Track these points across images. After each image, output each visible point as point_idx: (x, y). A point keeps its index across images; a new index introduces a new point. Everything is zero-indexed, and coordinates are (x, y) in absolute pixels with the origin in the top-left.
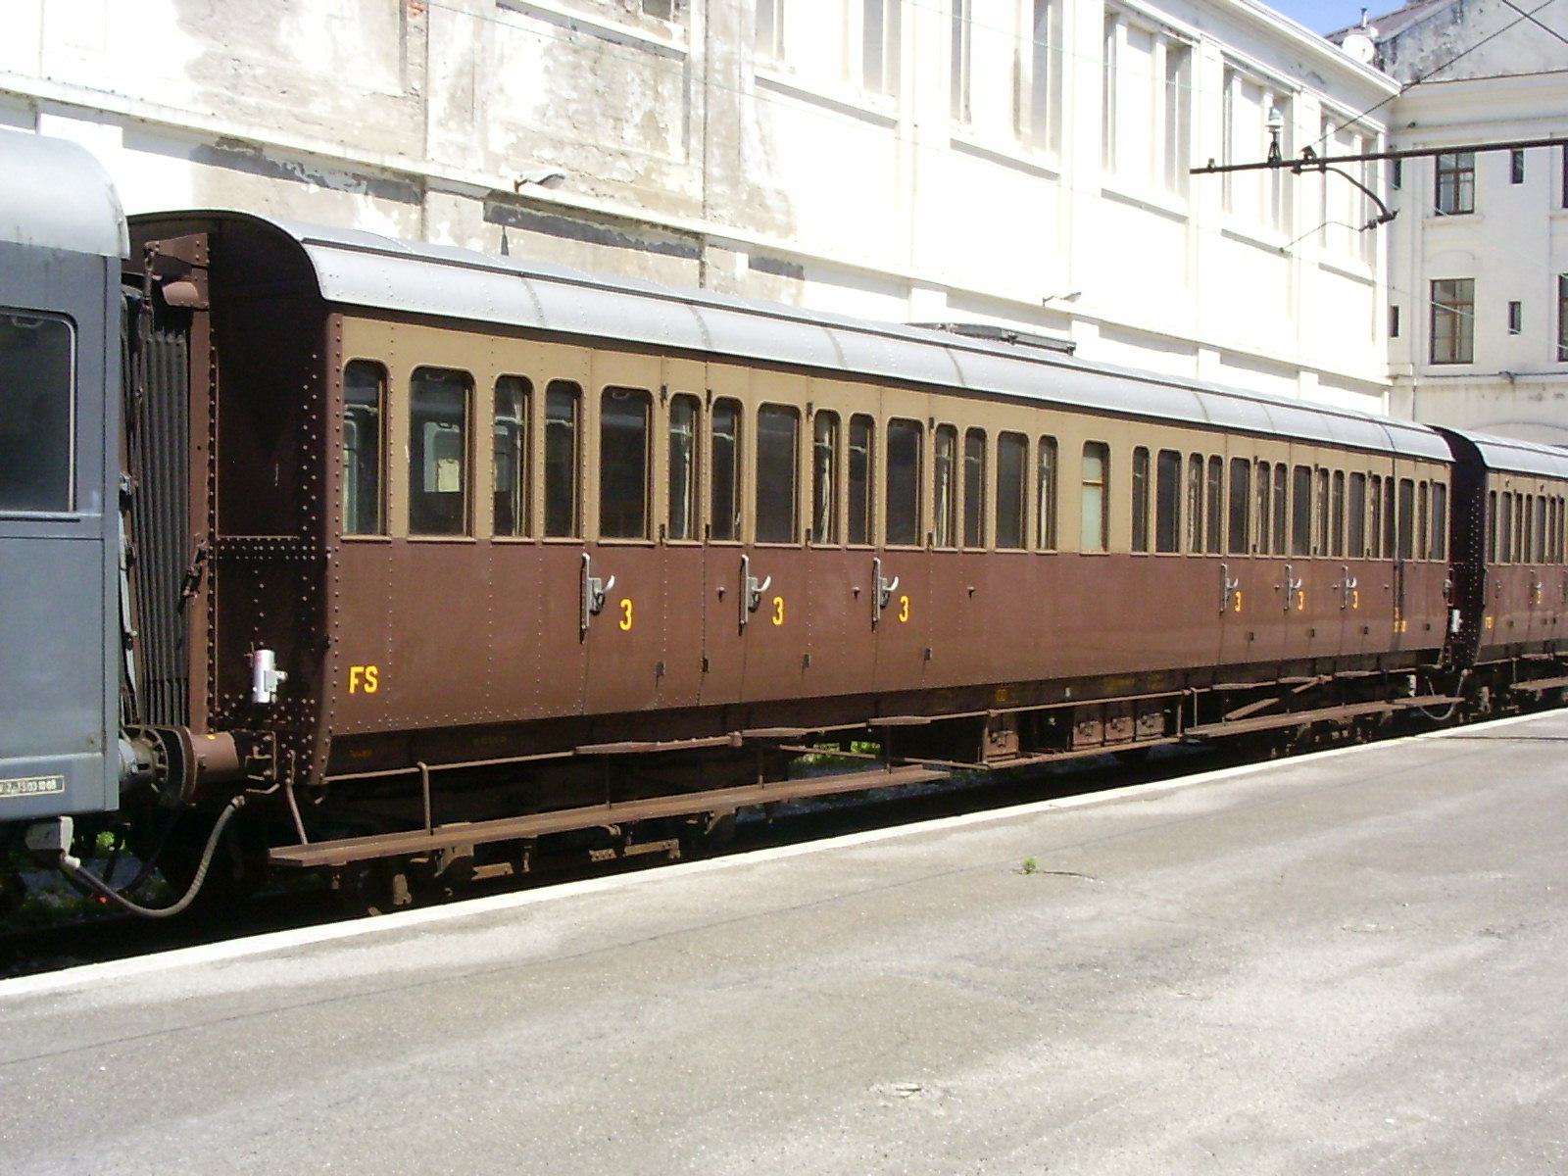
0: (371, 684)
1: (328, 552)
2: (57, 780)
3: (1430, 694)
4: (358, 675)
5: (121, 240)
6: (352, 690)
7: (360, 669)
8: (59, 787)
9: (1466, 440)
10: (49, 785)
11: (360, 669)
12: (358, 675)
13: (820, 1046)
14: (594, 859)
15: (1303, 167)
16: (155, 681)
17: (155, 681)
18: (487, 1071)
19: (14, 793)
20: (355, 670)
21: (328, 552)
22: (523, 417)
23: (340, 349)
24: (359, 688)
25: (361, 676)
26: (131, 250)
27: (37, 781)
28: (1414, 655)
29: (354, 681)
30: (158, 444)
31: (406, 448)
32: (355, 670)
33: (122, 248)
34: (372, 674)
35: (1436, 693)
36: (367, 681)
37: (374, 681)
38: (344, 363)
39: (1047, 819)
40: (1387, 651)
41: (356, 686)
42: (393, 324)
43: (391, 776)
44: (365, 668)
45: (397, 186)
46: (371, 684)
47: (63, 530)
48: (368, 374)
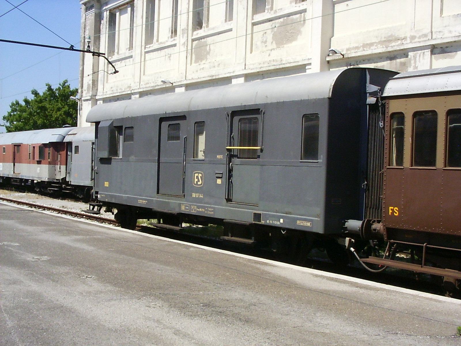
0: (396, 213)
2: (310, 223)
4: (391, 209)
5: (329, 93)
6: (390, 214)
7: (392, 208)
8: (310, 225)
10: (309, 224)
11: (392, 208)
12: (391, 209)
13: (12, 256)
16: (373, 208)
17: (373, 208)
18: (94, 259)
19: (302, 224)
20: (390, 208)
22: (313, 116)
23: (389, 110)
24: (393, 213)
26: (332, 95)
27: (307, 223)
29: (390, 211)
30: (372, 146)
31: (410, 138)
32: (390, 208)
33: (329, 95)
34: (396, 210)
36: (395, 212)
38: (390, 114)
39: (34, 214)
40: (107, 157)
41: (391, 213)
42: (407, 99)
43: (411, 245)
44: (394, 208)
46: (396, 213)
47: (315, 165)
48: (399, 117)
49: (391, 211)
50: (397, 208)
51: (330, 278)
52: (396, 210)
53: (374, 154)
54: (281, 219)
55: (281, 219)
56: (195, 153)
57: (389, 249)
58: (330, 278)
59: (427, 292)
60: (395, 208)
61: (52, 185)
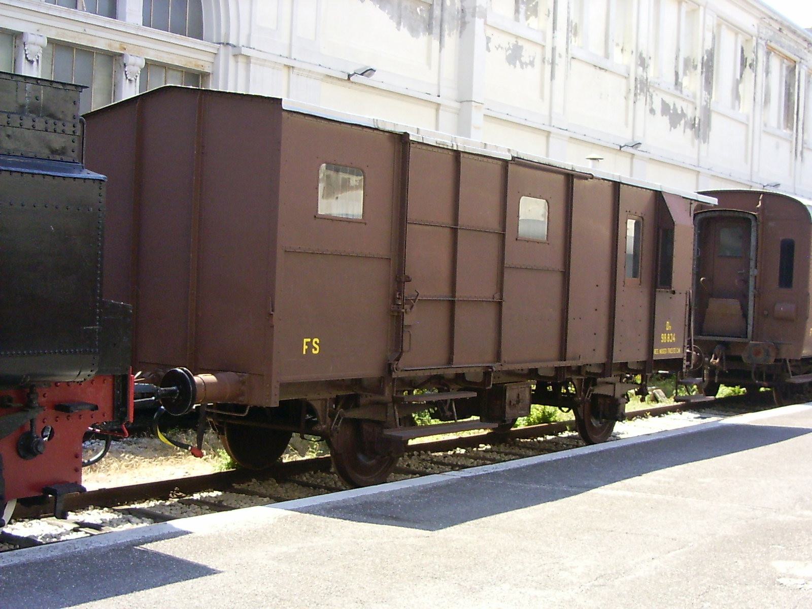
1: (667, 342)
3: (186, 36)
6: (304, 353)
7: (309, 340)
9: (801, 204)
11: (309, 340)
12: (307, 343)
14: (662, 335)
15: (599, 380)
20: (305, 340)
21: (667, 342)
24: (309, 351)
25: (309, 344)
28: (650, 193)
29: (305, 347)
32: (305, 340)
34: (316, 343)
35: (171, 32)
37: (317, 347)
45: (707, 71)
49: (307, 347)
50: (317, 340)
51: (455, 523)
52: (316, 343)
53: (797, 122)
54: (629, 221)
55: (629, 221)
56: (637, 225)
57: (119, 504)
58: (455, 523)
59: (167, 481)
60: (315, 340)
61: (212, 404)
